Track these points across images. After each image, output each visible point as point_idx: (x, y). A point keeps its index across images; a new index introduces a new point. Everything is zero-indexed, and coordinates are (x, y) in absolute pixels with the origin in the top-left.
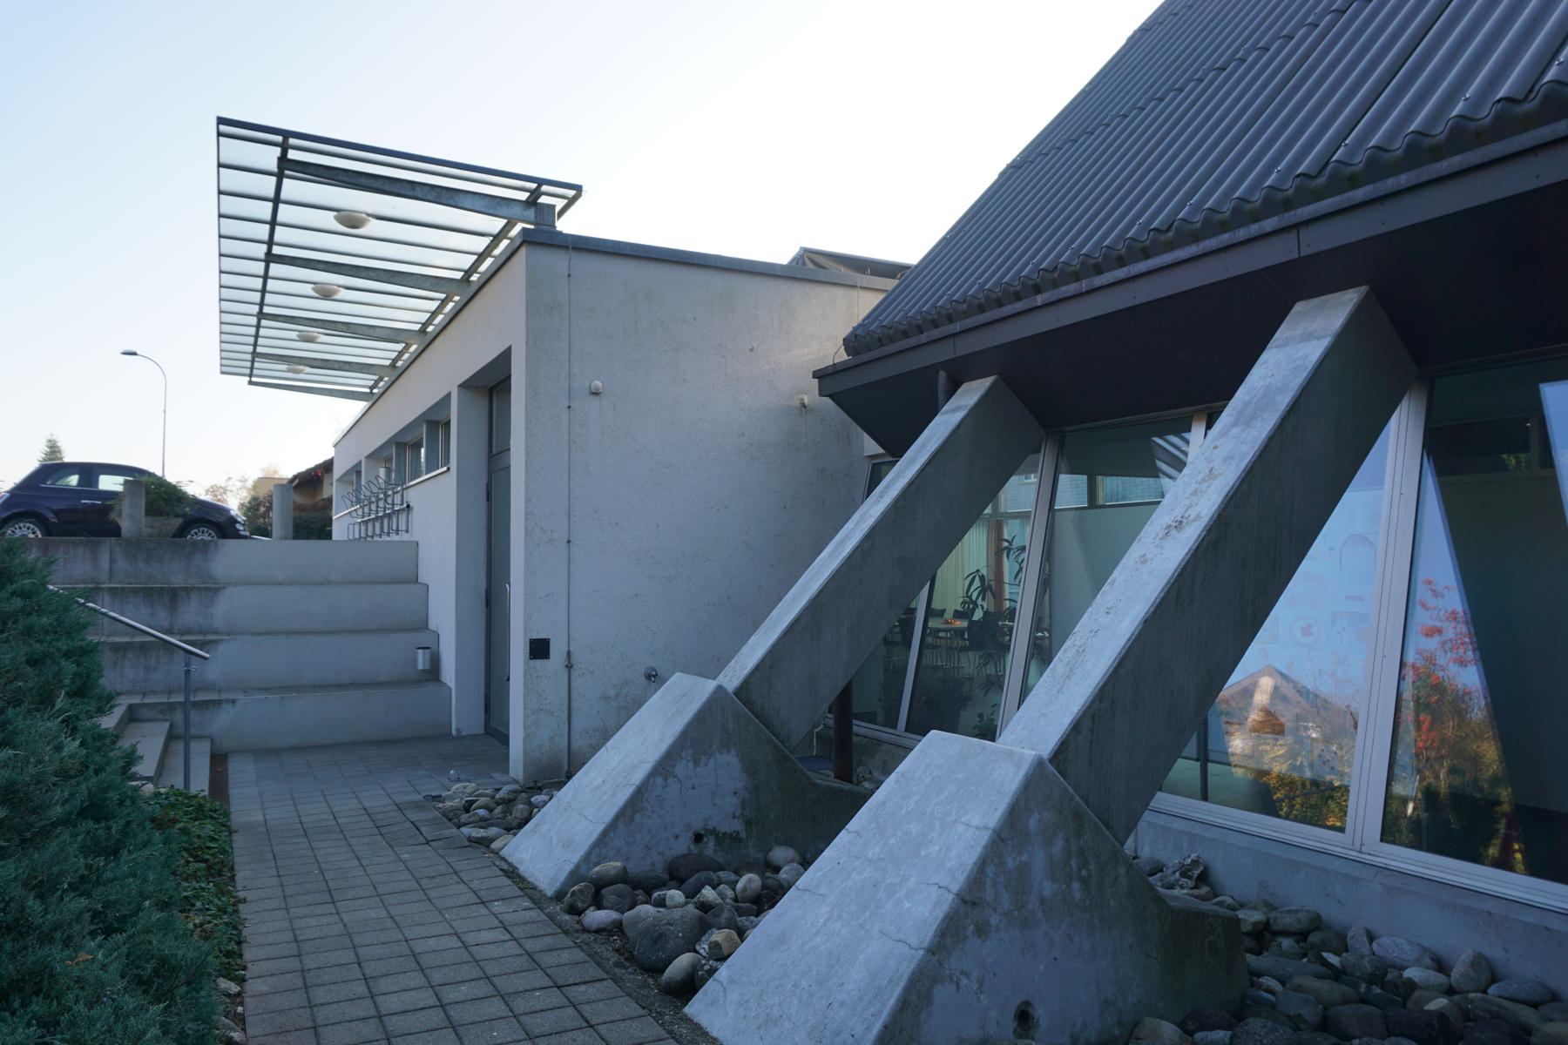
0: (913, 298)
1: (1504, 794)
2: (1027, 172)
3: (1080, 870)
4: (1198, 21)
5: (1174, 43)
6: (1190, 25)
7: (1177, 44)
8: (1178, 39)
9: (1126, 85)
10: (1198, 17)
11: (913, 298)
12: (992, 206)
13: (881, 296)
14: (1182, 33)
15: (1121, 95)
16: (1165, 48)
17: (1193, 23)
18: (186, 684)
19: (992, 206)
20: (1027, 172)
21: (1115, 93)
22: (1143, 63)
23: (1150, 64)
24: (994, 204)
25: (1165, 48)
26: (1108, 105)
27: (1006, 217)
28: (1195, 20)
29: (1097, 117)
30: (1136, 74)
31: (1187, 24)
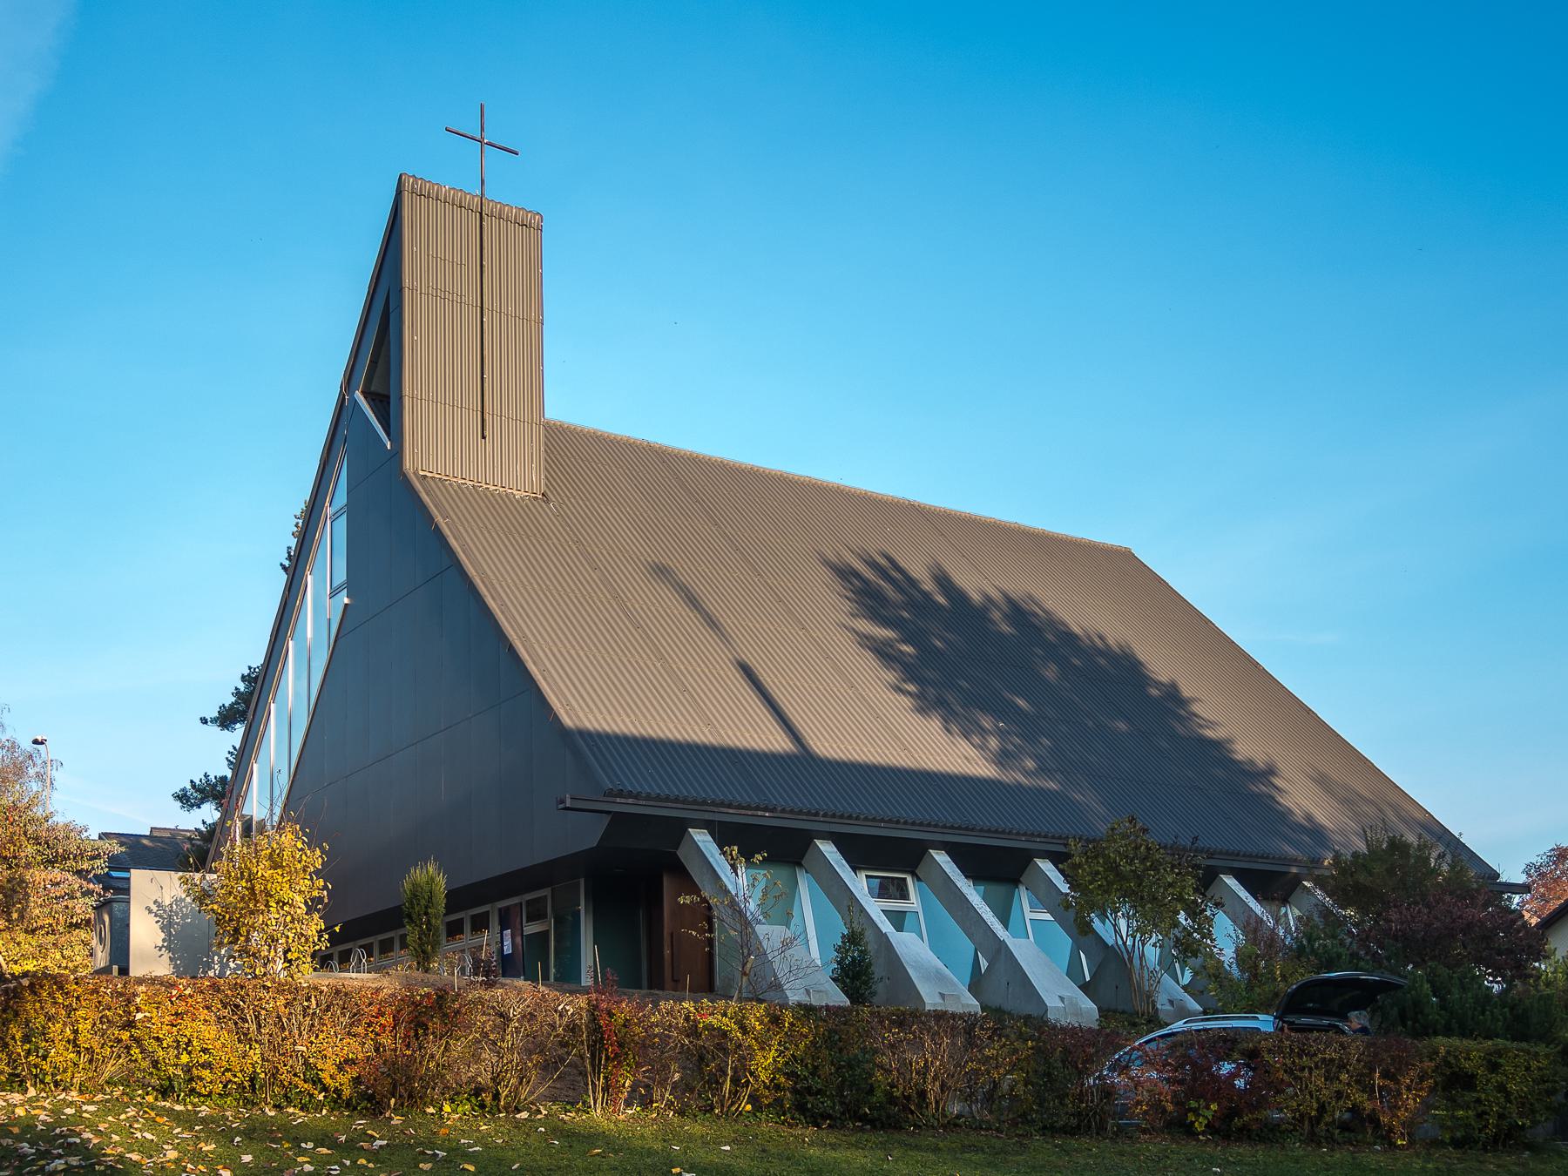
0: (807, 623)
1: (1367, 1124)
2: (588, 642)
3: (1294, 1060)
4: (824, 600)
5: (783, 645)
6: (771, 639)
7: (845, 658)
8: (577, 486)
9: (884, 786)
10: (879, 780)
11: (807, 623)
12: (656, 548)
13: (346, 513)
14: (767, 562)
15: (823, 667)
16: (647, 483)
17: (753, 587)
18: (890, 562)
19: (627, 518)
20: (588, 642)
21: (588, 578)
22: (528, 553)
23: (857, 665)
24: (665, 499)
25: (635, 540)
26: (867, 716)
27: (931, 746)
28: (704, 778)
29: (786, 599)
30: (820, 667)
31: (699, 546)
